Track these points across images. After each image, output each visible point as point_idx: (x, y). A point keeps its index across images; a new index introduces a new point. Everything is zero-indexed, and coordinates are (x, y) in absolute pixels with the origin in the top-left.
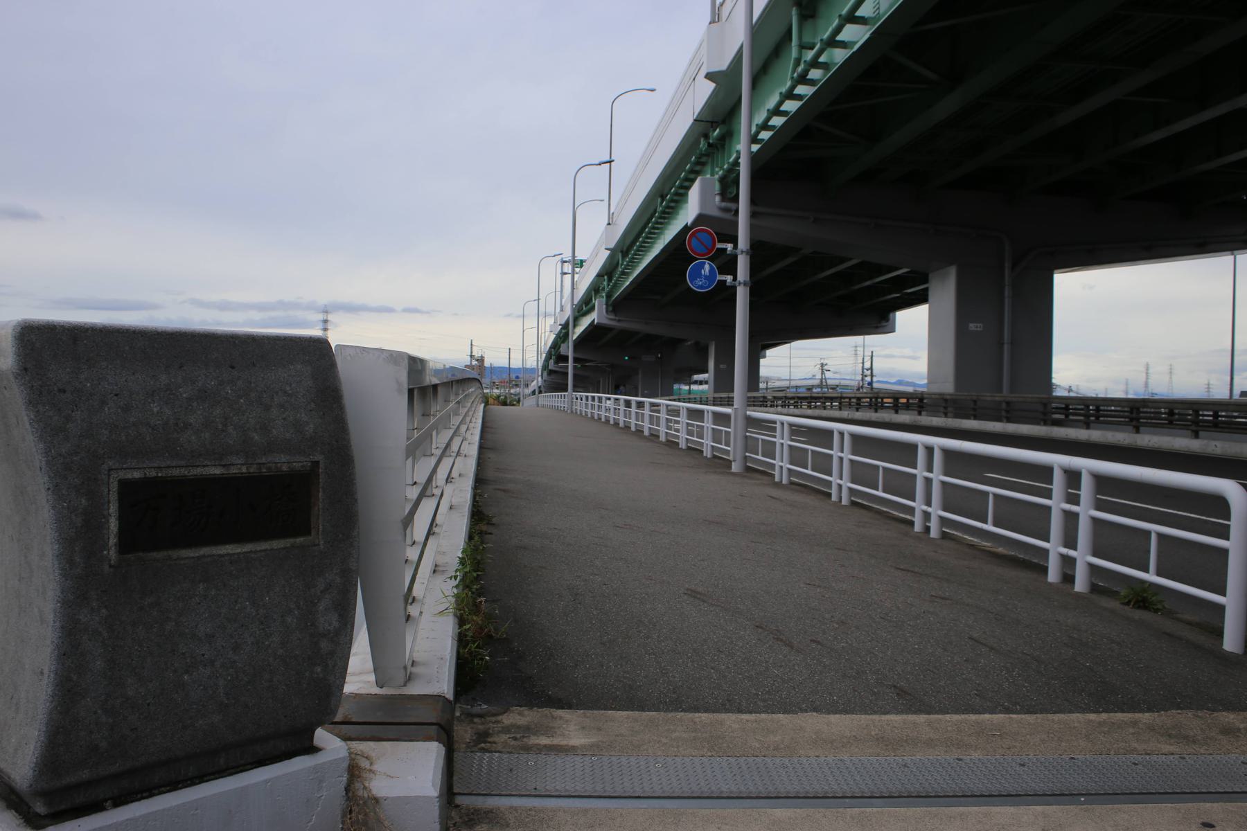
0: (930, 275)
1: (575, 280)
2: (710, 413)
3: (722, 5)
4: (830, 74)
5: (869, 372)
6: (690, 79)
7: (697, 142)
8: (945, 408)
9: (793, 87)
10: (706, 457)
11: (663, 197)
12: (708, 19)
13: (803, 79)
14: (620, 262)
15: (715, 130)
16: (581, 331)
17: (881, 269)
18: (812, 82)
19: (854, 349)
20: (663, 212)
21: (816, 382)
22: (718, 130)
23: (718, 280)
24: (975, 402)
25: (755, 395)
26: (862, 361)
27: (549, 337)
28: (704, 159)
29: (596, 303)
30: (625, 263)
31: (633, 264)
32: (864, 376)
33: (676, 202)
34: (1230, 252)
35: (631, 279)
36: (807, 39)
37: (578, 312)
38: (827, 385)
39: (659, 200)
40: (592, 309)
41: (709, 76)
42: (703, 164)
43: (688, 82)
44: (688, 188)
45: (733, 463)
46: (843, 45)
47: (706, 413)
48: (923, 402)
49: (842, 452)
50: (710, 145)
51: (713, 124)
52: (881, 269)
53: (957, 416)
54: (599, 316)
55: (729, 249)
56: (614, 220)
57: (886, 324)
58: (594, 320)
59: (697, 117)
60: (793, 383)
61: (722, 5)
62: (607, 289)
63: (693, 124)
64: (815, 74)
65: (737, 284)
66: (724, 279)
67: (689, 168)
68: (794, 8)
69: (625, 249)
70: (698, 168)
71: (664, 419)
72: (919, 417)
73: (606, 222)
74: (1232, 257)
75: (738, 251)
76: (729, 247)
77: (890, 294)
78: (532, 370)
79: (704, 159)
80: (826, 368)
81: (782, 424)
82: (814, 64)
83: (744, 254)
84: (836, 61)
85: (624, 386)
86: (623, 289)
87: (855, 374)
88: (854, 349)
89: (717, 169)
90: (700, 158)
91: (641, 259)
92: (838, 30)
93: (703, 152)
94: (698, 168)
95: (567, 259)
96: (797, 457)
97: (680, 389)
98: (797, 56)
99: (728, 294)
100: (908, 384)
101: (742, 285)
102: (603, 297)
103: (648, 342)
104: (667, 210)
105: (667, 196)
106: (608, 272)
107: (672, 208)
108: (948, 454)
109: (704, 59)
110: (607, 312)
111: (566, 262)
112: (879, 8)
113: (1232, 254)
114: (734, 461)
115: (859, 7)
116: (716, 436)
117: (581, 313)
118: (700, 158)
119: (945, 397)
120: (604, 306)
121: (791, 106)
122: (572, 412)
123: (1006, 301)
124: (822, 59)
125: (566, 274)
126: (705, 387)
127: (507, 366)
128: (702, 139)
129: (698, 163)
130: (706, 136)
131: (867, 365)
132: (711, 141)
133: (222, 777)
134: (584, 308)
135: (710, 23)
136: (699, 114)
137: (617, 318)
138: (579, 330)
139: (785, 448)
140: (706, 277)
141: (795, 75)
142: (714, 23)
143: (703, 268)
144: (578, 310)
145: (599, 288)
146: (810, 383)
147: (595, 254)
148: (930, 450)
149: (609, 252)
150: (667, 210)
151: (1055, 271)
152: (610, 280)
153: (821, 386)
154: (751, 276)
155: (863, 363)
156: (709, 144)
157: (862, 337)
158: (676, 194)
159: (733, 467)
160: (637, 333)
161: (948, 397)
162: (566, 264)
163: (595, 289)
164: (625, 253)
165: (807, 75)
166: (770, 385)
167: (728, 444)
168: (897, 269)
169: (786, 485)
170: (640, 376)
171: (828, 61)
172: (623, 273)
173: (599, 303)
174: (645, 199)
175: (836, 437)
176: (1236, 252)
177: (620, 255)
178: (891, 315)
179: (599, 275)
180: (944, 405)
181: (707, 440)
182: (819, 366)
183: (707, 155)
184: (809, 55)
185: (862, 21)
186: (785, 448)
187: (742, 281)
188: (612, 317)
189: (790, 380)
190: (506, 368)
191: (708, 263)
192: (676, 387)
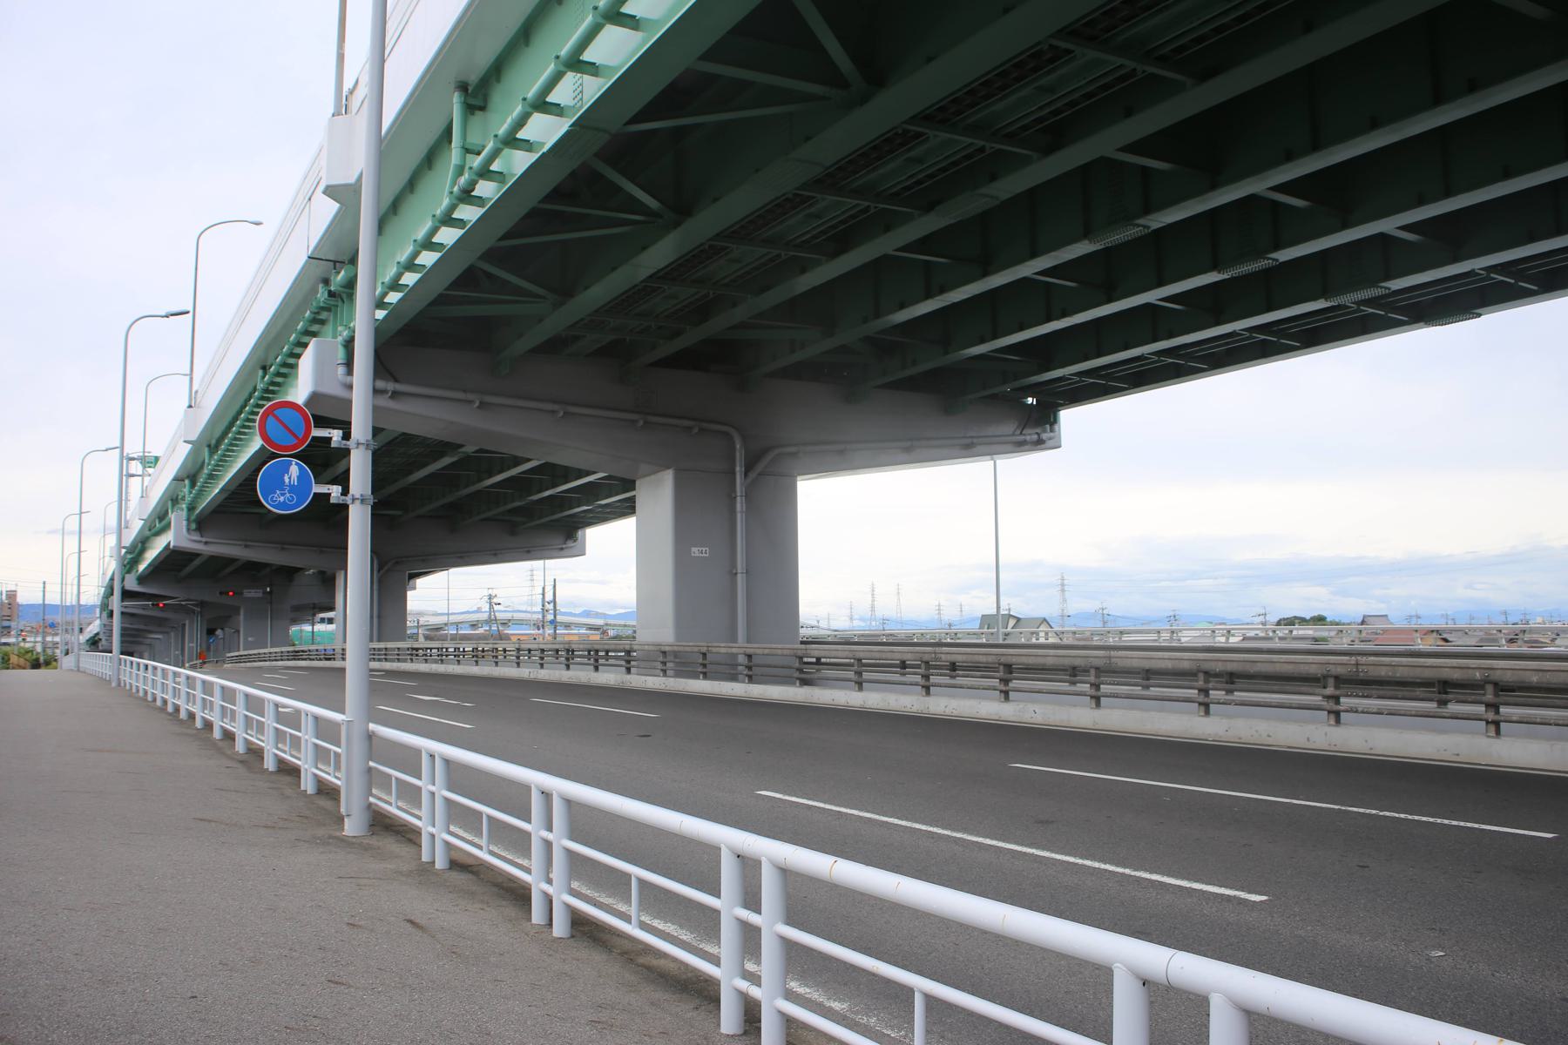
0: (638, 483)
1: (145, 485)
3: (351, 92)
4: (507, 187)
5: (551, 606)
6: (304, 198)
7: (314, 291)
8: (664, 663)
9: (453, 208)
11: (265, 368)
12: (332, 111)
13: (467, 196)
14: (207, 461)
15: (339, 273)
16: (153, 557)
17: (567, 473)
18: (479, 201)
19: (529, 573)
20: (266, 391)
21: (485, 616)
22: (343, 273)
23: (315, 493)
24: (704, 655)
25: (399, 646)
26: (541, 592)
27: (108, 565)
28: (324, 315)
29: (172, 516)
31: (223, 462)
32: (544, 611)
33: (284, 376)
34: (989, 457)
35: (222, 484)
36: (474, 139)
37: (150, 530)
38: (496, 620)
39: (260, 373)
40: (166, 528)
41: (331, 191)
42: (323, 322)
43: (302, 203)
44: (298, 356)
45: (346, 820)
46: (527, 145)
48: (630, 656)
50: (331, 294)
51: (336, 264)
52: (567, 473)
53: (679, 674)
54: (176, 537)
55: (334, 439)
56: (198, 400)
57: (574, 544)
58: (169, 543)
59: (311, 254)
60: (453, 619)
61: (351, 92)
62: (188, 499)
63: (307, 261)
64: (486, 189)
65: (349, 502)
66: (327, 491)
67: (302, 327)
68: (456, 94)
69: (213, 442)
70: (315, 328)
72: (628, 677)
73: (187, 405)
75: (351, 444)
76: (336, 435)
77: (579, 506)
78: (91, 608)
79: (324, 315)
80: (495, 600)
81: (432, 756)
82: (485, 173)
83: (362, 448)
84: (515, 172)
85: (222, 629)
86: (209, 499)
87: (532, 605)
88: (529, 573)
89: (340, 328)
90: (318, 313)
91: (236, 457)
92: (521, 122)
93: (322, 305)
94: (315, 328)
95: (135, 456)
97: (301, 631)
98: (458, 163)
99: (330, 517)
100: (597, 615)
101: (358, 502)
102: (183, 510)
103: (251, 571)
104: (271, 388)
105: (271, 367)
106: (190, 475)
107: (278, 384)
109: (323, 174)
110: (188, 530)
111: (133, 459)
112: (581, 92)
113: (992, 459)
115: (551, 91)
116: (321, 755)
117: (153, 531)
118: (318, 313)
119: (663, 649)
120: (185, 523)
121: (448, 236)
122: (119, 684)
123: (739, 515)
124: (494, 167)
125: (133, 476)
126: (331, 627)
127: (41, 602)
128: (321, 286)
129: (315, 321)
130: (326, 282)
131: (549, 597)
132: (332, 288)
134: (157, 525)
135: (333, 115)
136: (316, 248)
137: (204, 540)
138: (151, 555)
139: (439, 802)
140: (292, 488)
141: (456, 189)
142: (339, 115)
143: (287, 471)
144: (150, 526)
145: (178, 496)
146: (474, 617)
147: (172, 449)
148: (547, 795)
149: (190, 446)
150: (271, 388)
151: (799, 478)
152: (193, 484)
153: (489, 621)
154: (374, 489)
155: (543, 595)
156: (330, 292)
157: (541, 562)
158: (285, 365)
159: (346, 827)
160: (232, 561)
161: (667, 649)
162: (134, 462)
163: (172, 499)
164: (213, 449)
165: (473, 190)
166: (423, 620)
168: (588, 473)
170: (242, 617)
171: (505, 171)
172: (211, 476)
173: (178, 518)
177: (206, 450)
178: (580, 533)
179: (178, 479)
180: (661, 659)
182: (486, 598)
183: (328, 309)
184: (476, 161)
185: (556, 110)
186: (439, 802)
187: (358, 496)
188: (197, 538)
189: (448, 614)
190: (39, 605)
191: (297, 464)
192: (294, 629)
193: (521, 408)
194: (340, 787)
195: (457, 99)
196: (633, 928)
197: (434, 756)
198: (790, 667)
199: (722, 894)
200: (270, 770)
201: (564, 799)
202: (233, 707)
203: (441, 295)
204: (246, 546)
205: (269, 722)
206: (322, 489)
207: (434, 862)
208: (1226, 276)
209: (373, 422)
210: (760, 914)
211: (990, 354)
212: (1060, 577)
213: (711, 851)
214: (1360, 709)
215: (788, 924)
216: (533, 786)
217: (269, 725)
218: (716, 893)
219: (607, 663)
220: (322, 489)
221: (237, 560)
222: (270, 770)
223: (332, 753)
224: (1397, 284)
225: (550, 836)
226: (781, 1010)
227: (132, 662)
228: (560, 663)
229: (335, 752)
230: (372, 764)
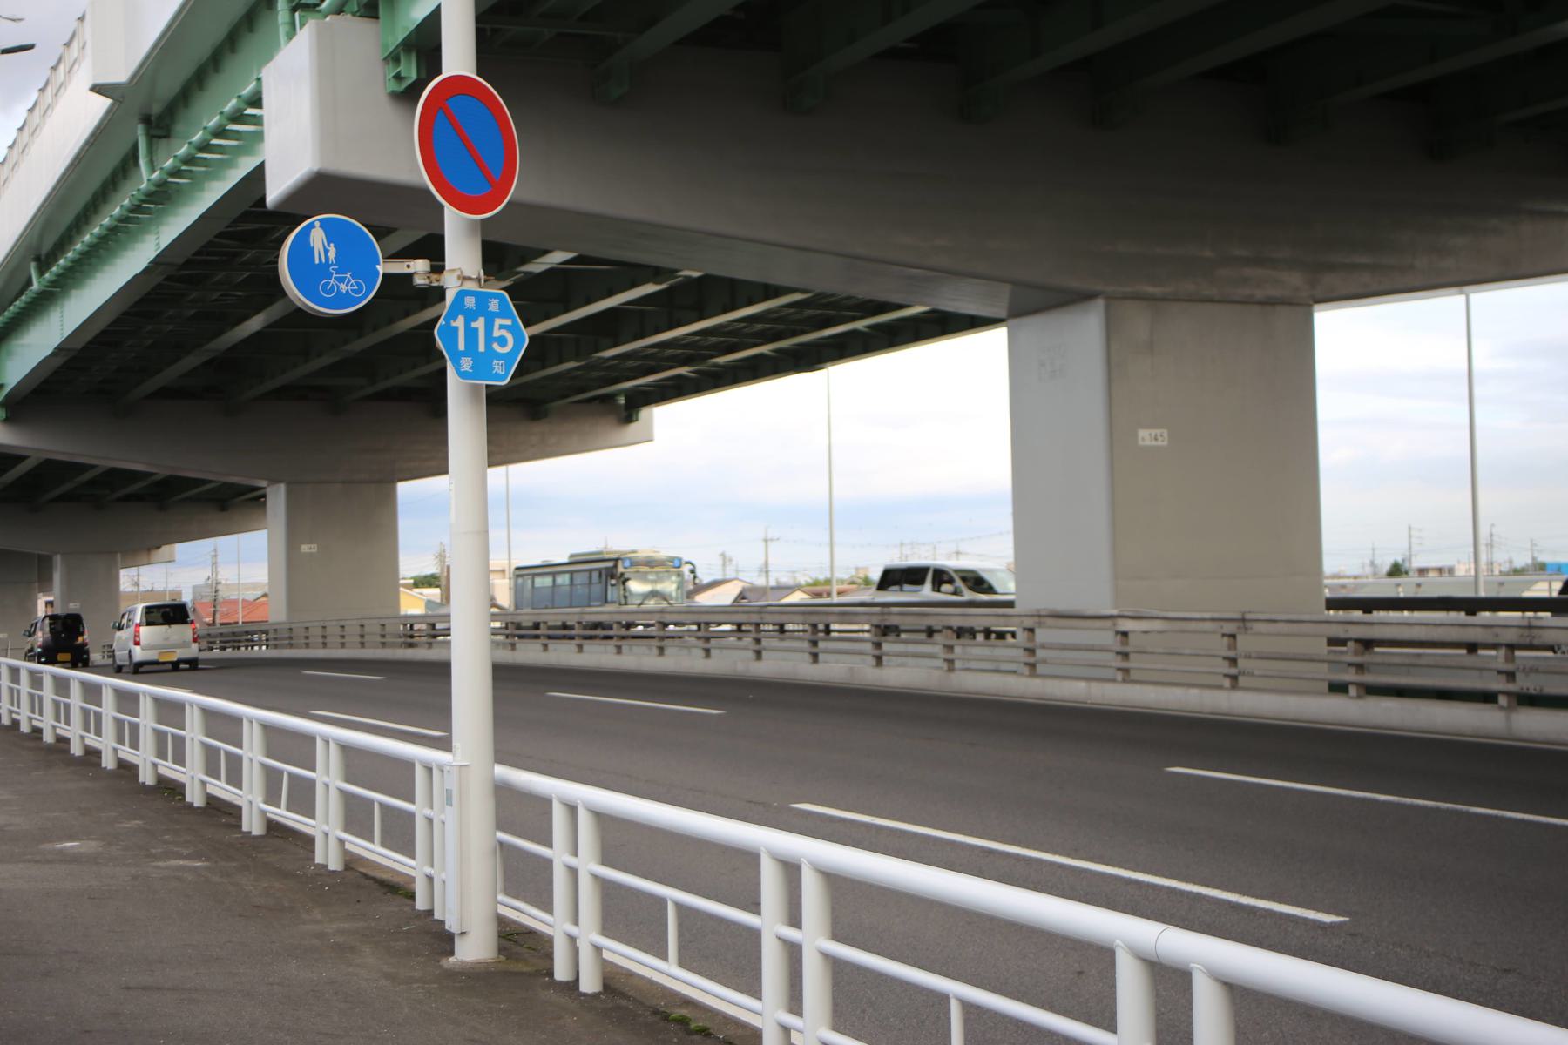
2: (332, 746)
10: (325, 866)
47: (245, 724)
49: (575, 853)
66: (407, 271)
74: (1463, 297)
96: (356, 816)
108: (838, 885)
113: (1461, 293)
133: (11, 251)
148: (791, 870)
149: (103, 103)
169: (595, 996)
174: (54, 189)
175: (559, 816)
176: (1467, 289)
181: (251, 792)
195: (140, 130)
198: (1103, 650)
199: (317, 768)
200: (254, 833)
201: (589, 810)
202: (66, 700)
203: (210, 243)
206: (399, 267)
212: (212, 549)
213: (749, 859)
214: (1253, 655)
218: (412, 801)
219: (628, 633)
220: (399, 267)
228: (745, 648)
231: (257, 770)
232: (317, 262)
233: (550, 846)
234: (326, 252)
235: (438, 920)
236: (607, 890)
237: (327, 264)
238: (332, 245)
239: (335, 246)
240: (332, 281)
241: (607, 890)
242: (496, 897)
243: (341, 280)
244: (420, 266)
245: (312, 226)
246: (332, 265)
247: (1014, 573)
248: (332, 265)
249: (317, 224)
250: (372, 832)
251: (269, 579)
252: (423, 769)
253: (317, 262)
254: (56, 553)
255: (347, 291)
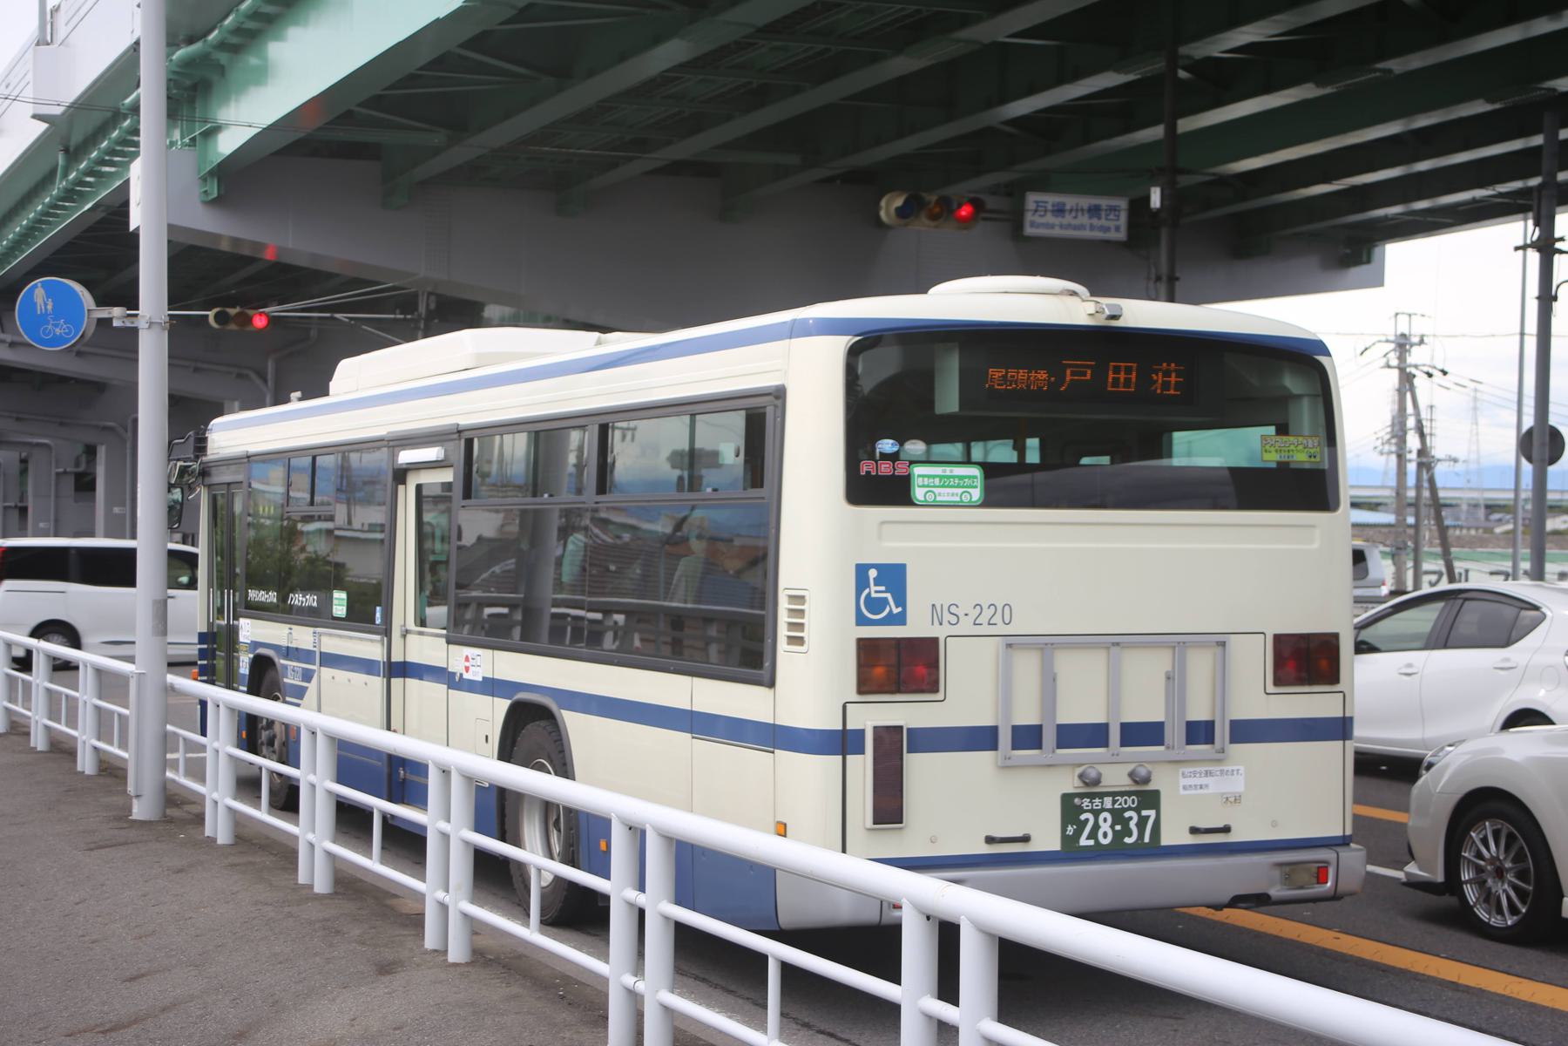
2: (321, 740)
10: (214, 840)
30: (72, 176)
45: (135, 802)
49: (641, 887)
71: (89, 708)
75: (141, 324)
81: (446, 773)
83: (156, 329)
114: (138, 796)
148: (638, 834)
149: (44, 126)
159: (135, 810)
167: (123, 745)
193: (113, 357)
194: (125, 760)
196: (532, 932)
197: (643, 833)
200: (39, 749)
201: (463, 776)
204: (18, 419)
205: (38, 681)
207: (445, 952)
208: (1131, 77)
209: (168, 236)
210: (609, 879)
211: (1071, 103)
215: (476, 831)
216: (430, 762)
217: (38, 685)
220: (104, 313)
221: (337, 275)
222: (220, 841)
223: (20, 681)
224: (1397, 65)
225: (641, 899)
226: (465, 912)
227: (947, 935)
229: (120, 715)
230: (169, 728)
231: (42, 693)
232: (39, 313)
233: (895, 978)
234: (46, 305)
235: (80, 772)
236: (685, 937)
237: (46, 314)
238: (50, 300)
239: (52, 301)
240: (50, 327)
241: (685, 937)
242: (165, 773)
243: (56, 326)
244: (117, 312)
245: (35, 286)
246: (50, 314)
247: (324, 558)
248: (50, 314)
249: (39, 285)
250: (113, 740)
251: (958, 442)
252: (461, 778)
253: (39, 313)
254: (102, 444)
255: (61, 333)
